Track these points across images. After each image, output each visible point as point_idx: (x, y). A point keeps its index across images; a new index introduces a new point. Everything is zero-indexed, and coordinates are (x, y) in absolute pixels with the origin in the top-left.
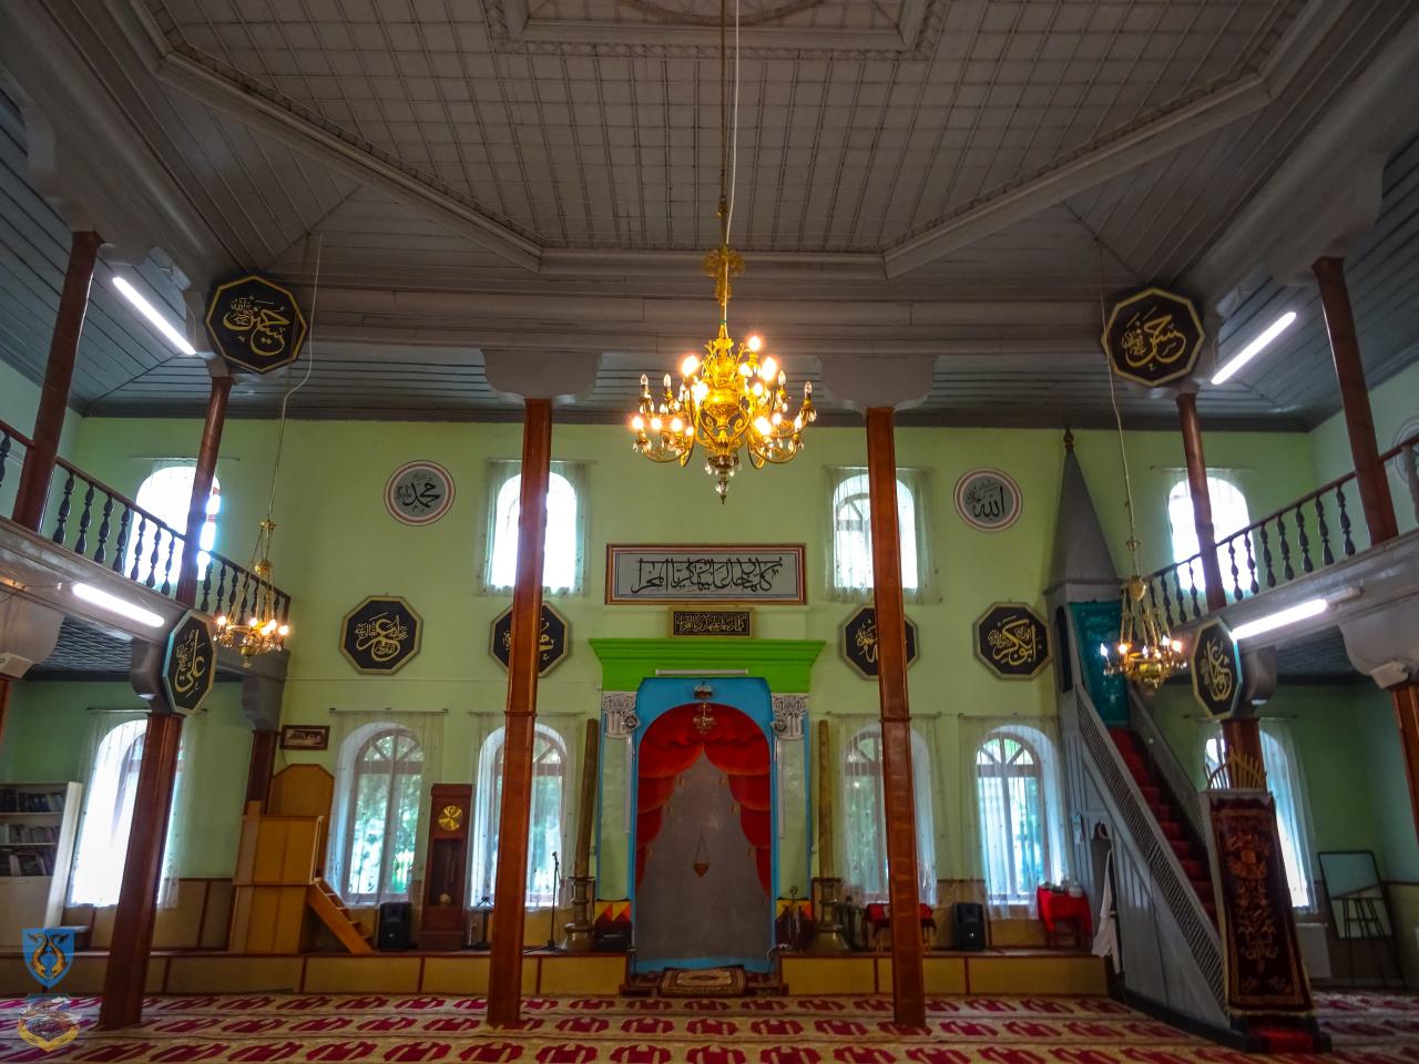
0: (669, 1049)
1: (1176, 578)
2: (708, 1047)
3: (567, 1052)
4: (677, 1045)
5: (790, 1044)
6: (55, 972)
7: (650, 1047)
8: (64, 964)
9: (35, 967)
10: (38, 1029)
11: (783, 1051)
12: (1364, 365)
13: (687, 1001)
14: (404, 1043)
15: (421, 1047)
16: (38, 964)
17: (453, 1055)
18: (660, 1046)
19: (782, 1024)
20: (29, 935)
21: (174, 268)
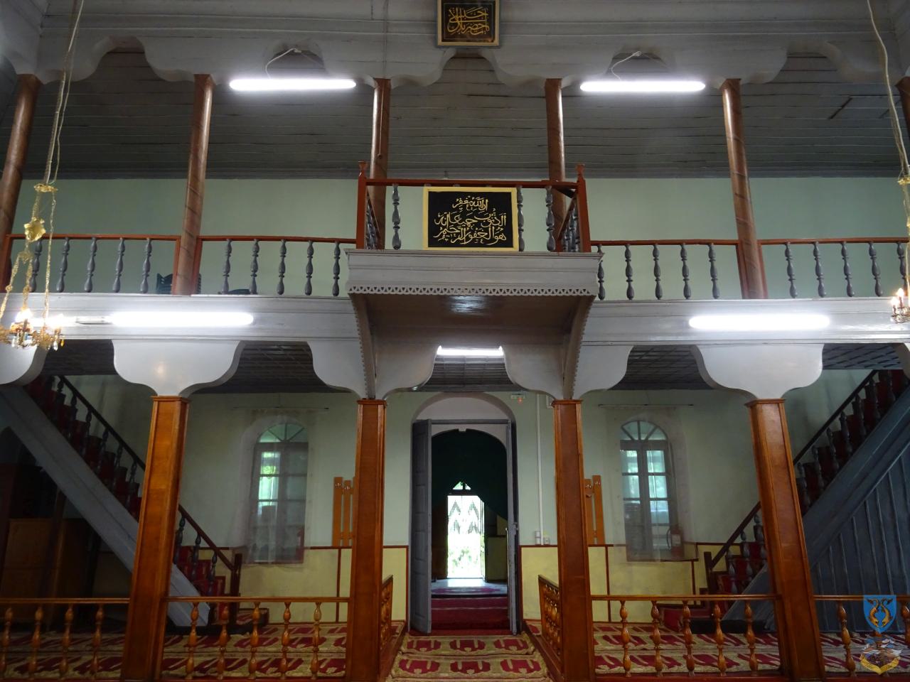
0: (452, 650)
1: (211, 79)
2: (422, 673)
3: (335, 667)
4: (447, 675)
5: (510, 652)
6: (884, 623)
7: (413, 672)
8: (890, 618)
9: (871, 620)
10: (872, 659)
11: (516, 648)
12: (567, 197)
13: (826, 430)
14: (266, 648)
15: (204, 645)
16: (873, 618)
17: (445, 671)
18: (458, 652)
19: (462, 648)
20: (869, 601)
21: (36, 345)
